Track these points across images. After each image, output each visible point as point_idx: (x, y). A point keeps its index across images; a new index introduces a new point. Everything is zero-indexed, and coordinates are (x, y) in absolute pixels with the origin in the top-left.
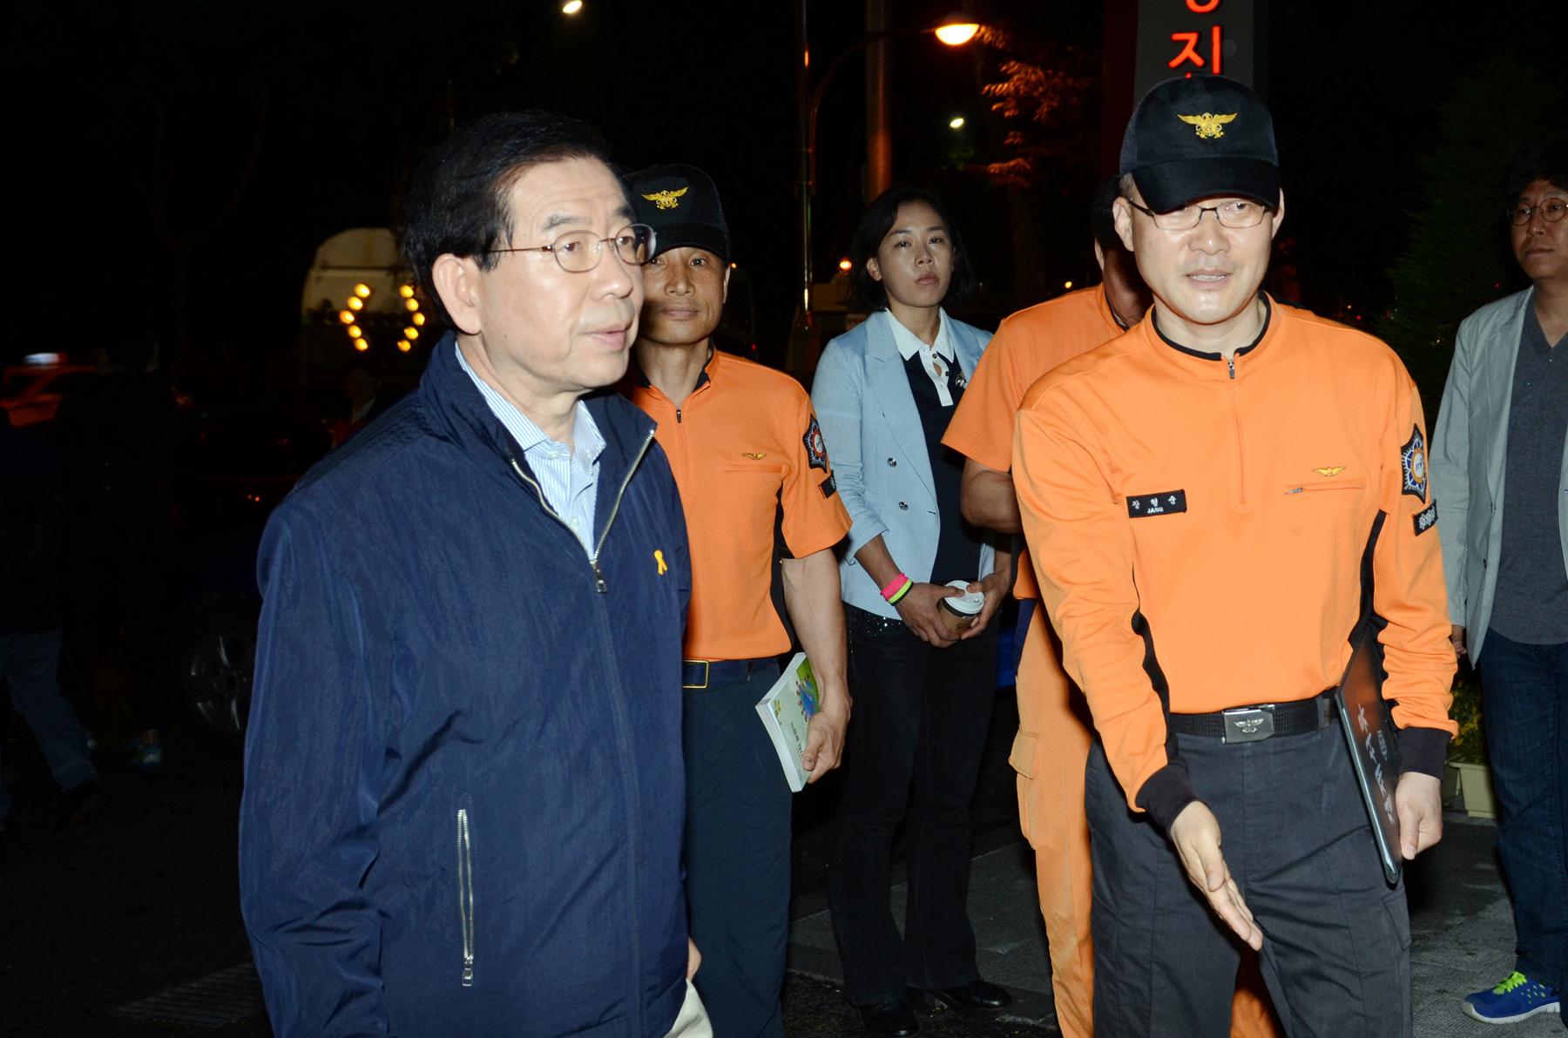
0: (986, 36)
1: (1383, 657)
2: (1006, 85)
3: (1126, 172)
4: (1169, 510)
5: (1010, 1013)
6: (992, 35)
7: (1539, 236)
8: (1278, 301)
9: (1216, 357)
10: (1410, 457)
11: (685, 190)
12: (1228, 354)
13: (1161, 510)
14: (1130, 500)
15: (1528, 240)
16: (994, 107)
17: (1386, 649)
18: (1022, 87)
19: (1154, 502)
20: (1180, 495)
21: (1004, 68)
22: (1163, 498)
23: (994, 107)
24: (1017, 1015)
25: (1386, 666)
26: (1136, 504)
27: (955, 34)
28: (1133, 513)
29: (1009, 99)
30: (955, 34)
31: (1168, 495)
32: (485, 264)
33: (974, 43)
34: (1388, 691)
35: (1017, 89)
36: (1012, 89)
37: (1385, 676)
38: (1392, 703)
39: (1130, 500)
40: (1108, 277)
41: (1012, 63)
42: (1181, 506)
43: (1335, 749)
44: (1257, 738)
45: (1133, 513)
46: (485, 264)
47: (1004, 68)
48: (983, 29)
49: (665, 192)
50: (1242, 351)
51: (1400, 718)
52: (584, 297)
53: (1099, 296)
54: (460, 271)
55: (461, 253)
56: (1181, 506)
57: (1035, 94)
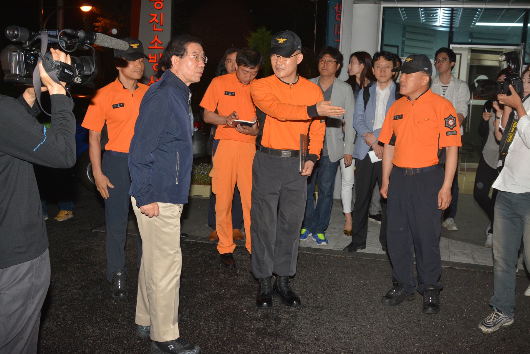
0: (94, 10)
1: (310, 142)
2: (100, 23)
3: (449, 46)
4: (121, 106)
5: (188, 239)
6: (96, 10)
7: (326, 66)
8: (300, 76)
9: (288, 84)
10: (448, 120)
11: (138, 44)
12: (291, 84)
13: (119, 106)
14: (225, 92)
15: (323, 67)
16: (95, 29)
17: (310, 141)
18: (104, 24)
19: (118, 105)
20: (123, 103)
21: (98, 19)
22: (120, 104)
23: (95, 29)
24: (190, 239)
25: (310, 143)
26: (227, 93)
27: (86, 9)
28: (225, 94)
29: (100, 27)
30: (86, 9)
31: (121, 104)
32: (181, 58)
33: (91, 12)
34: (309, 147)
35: (102, 24)
36: (101, 24)
37: (309, 145)
38: (309, 150)
39: (225, 92)
40: (239, 71)
41: (100, 18)
42: (123, 106)
43: (454, 101)
44: (287, 157)
45: (225, 94)
46: (181, 58)
47: (98, 19)
48: (93, 8)
49: (134, 44)
50: (293, 84)
51: (310, 152)
52: (197, 67)
53: (234, 75)
54: (176, 59)
55: (177, 55)
56: (123, 106)
57: (107, 26)
